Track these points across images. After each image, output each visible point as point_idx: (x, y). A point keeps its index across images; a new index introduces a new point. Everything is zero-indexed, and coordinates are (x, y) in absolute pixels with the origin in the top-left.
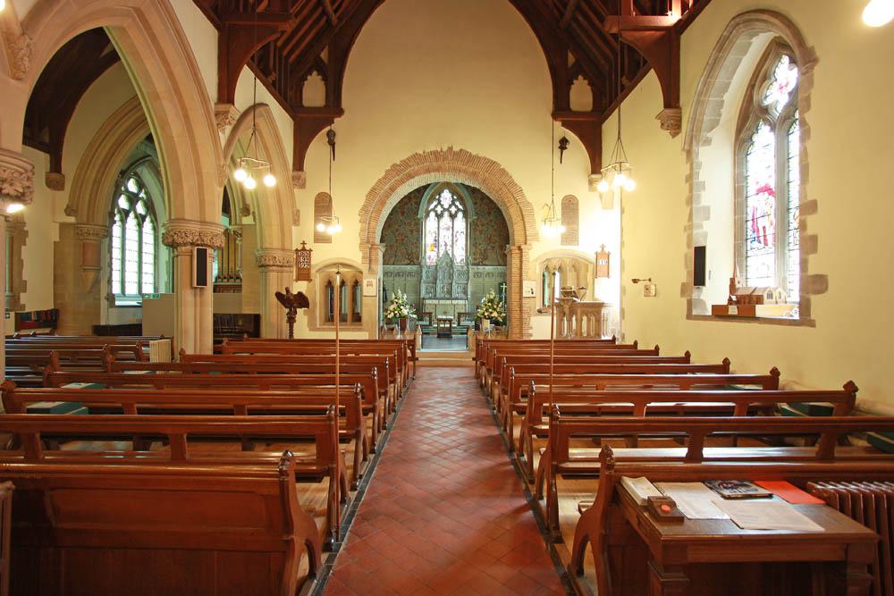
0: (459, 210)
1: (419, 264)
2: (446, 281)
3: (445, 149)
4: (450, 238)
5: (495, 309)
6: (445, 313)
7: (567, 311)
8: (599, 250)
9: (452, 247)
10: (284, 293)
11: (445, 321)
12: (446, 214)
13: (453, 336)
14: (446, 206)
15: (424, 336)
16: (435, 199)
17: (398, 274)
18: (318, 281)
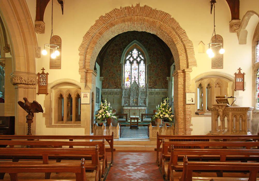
0: (141, 59)
1: (121, 88)
2: (135, 97)
3: (134, 5)
4: (137, 74)
5: (166, 112)
6: (134, 114)
7: (221, 113)
8: (237, 72)
9: (138, 79)
10: (24, 101)
11: (134, 119)
12: (135, 62)
13: (139, 127)
14: (135, 57)
15: (123, 127)
16: (129, 54)
17: (110, 94)
18: (53, 94)
